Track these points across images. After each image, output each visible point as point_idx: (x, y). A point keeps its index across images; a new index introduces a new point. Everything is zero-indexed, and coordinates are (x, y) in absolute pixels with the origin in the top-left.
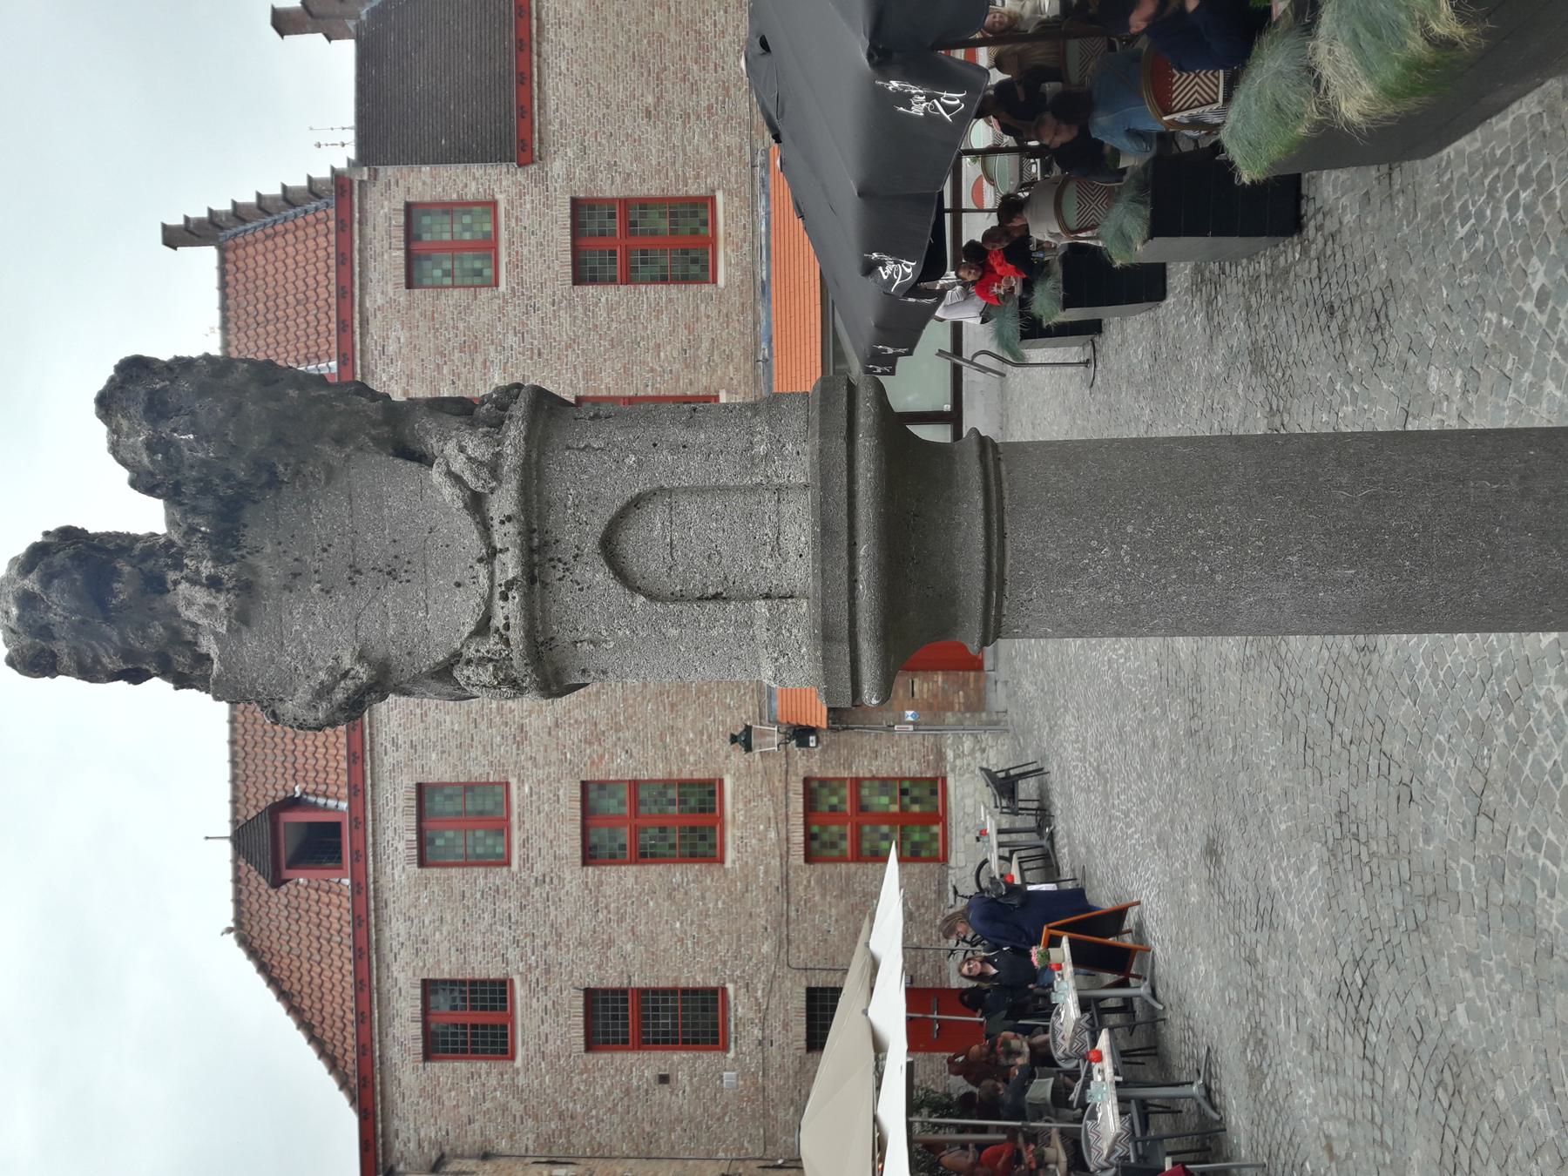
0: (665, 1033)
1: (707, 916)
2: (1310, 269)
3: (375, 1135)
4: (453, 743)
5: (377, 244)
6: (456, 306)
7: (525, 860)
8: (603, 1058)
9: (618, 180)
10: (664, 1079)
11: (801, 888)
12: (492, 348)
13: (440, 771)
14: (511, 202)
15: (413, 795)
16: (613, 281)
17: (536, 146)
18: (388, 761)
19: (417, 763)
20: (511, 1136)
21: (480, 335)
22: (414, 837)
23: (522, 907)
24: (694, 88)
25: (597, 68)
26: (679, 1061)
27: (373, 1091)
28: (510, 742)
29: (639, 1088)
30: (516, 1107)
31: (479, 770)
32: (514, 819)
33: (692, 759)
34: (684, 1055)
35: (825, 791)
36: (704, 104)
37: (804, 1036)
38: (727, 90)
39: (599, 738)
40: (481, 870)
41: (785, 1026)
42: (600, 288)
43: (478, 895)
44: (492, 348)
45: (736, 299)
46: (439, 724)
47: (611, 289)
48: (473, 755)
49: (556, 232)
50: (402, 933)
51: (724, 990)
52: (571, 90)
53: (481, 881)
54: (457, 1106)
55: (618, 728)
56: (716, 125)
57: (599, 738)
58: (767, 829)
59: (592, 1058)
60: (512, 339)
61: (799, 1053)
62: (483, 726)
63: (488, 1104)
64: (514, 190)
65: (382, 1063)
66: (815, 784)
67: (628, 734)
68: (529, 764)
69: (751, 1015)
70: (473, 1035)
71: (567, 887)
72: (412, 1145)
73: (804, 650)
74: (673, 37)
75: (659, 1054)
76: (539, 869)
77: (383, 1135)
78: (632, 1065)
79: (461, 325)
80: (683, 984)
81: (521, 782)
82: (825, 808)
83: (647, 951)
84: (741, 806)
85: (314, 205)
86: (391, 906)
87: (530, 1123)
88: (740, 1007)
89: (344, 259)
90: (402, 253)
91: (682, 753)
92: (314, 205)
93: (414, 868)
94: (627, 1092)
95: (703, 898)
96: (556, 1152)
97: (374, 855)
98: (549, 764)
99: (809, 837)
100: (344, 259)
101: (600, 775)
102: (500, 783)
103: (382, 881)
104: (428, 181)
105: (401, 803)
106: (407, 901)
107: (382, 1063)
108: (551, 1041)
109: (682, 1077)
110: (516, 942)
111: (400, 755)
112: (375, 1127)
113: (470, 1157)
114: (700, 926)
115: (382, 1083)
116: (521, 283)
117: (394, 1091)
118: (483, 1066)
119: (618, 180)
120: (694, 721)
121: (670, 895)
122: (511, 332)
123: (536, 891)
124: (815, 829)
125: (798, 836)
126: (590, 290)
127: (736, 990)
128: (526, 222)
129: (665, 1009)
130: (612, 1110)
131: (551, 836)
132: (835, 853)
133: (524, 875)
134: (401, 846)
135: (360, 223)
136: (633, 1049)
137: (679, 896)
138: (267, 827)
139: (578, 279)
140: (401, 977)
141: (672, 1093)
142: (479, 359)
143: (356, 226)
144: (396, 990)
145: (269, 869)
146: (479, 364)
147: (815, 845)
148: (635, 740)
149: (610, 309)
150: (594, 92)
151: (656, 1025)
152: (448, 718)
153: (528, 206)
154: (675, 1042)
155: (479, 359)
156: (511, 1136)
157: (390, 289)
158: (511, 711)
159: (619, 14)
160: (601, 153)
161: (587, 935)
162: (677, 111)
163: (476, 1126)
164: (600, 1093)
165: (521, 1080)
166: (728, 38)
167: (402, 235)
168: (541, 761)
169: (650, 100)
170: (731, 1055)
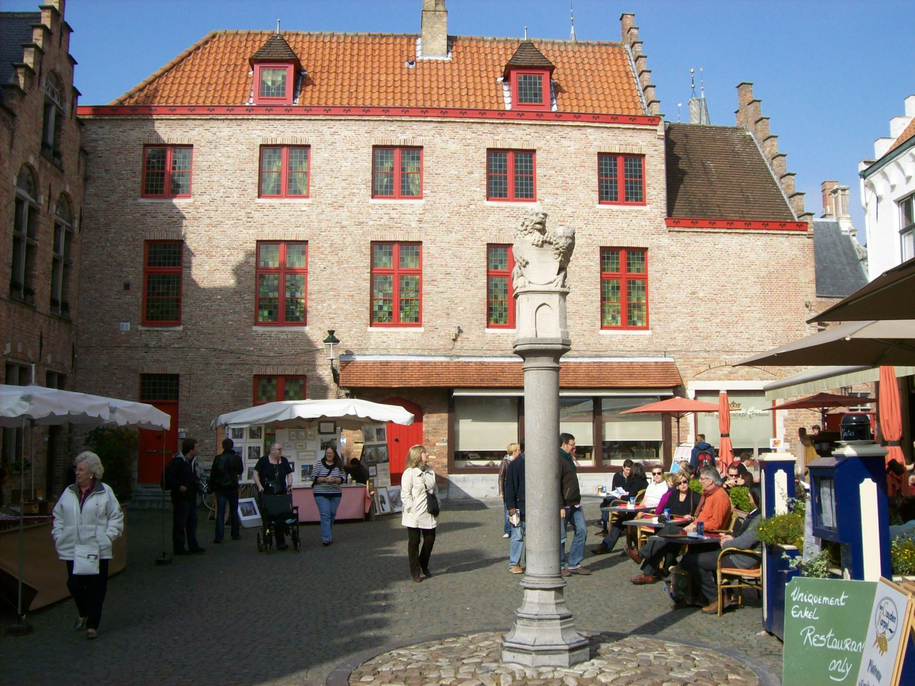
0: (154, 288)
1: (224, 315)
2: (198, 143)
3: (102, 115)
4: (334, 167)
5: (622, 137)
6: (588, 180)
7: (262, 207)
8: (141, 250)
9: (658, 275)
10: (127, 286)
11: (239, 372)
12: (565, 199)
13: (317, 158)
14: (645, 213)
15: (303, 143)
16: (602, 270)
17: (676, 229)
18: (325, 129)
19: (323, 146)
20: (96, 195)
21: (572, 192)
22: (278, 143)
23: (233, 204)
24: (707, 319)
25: (718, 265)
26: (136, 297)
27: (128, 115)
28: (334, 200)
29: (122, 272)
30: (114, 198)
31: (317, 181)
32: (287, 201)
33: (319, 307)
34: (141, 300)
35: (297, 388)
36: (699, 325)
37: (150, 372)
38: (706, 338)
39: (334, 252)
40: (257, 181)
41: (157, 361)
42: (599, 262)
43: (242, 179)
44: (565, 199)
45: (592, 341)
46: (345, 159)
47: (598, 268)
48: (326, 178)
49: (629, 238)
50: (222, 134)
51: (179, 324)
52: (706, 250)
53: (250, 181)
54: (116, 163)
55: (340, 263)
56: (687, 331)
57: (334, 252)
58: (275, 352)
59: (141, 243)
60: (569, 210)
61: (140, 369)
62: (344, 184)
63: (116, 181)
64: (652, 215)
65: (144, 120)
66: (301, 382)
67: (335, 269)
68: (319, 210)
69: (163, 340)
70: (158, 174)
71: (244, 231)
72: (94, 136)
73: (616, 649)
74: (734, 309)
75: (141, 285)
76: (256, 215)
77: (101, 120)
78: (136, 268)
79: (577, 182)
80: (184, 299)
81: (309, 205)
82: (287, 388)
83: (204, 278)
84: (290, 336)
85: (644, 101)
86: (239, 128)
87: (104, 206)
88: (169, 333)
89: (614, 118)
90: (617, 151)
91: (323, 301)
92: (644, 101)
93: (260, 142)
94: (120, 265)
95: (235, 313)
96: (86, 221)
97: (269, 119)
98: (320, 221)
99: (270, 378)
100: (614, 118)
101: (311, 252)
102: (308, 193)
103: (253, 123)
104: (657, 168)
105: (299, 136)
106: (241, 137)
107: (144, 120)
108: (152, 220)
109: (128, 298)
110: (213, 200)
111: (327, 136)
112: (106, 115)
113: (86, 171)
114: (218, 310)
115: (132, 120)
116: (601, 217)
117: (128, 125)
118: (139, 179)
119: (658, 275)
120: (342, 309)
121: (237, 292)
122: (574, 210)
123: (243, 213)
124: (274, 382)
125: (270, 371)
126: (598, 256)
127: (178, 331)
128: (634, 221)
129: (168, 288)
130: (109, 255)
131: (275, 222)
132: (260, 394)
133: (253, 206)
134: (273, 135)
135: (634, 129)
136: (145, 269)
137: (237, 298)
138: (287, 57)
139: (603, 249)
140: (195, 133)
141: (118, 292)
142: (559, 191)
143: (632, 126)
144: (187, 129)
145: (263, 56)
146: (555, 191)
147: (265, 382)
148: (332, 273)
149: (587, 267)
150: (705, 263)
151: (159, 283)
152: (349, 164)
153: (643, 223)
154: (149, 294)
155: (559, 191)
156: (96, 195)
157: (597, 143)
158: (352, 201)
159: (746, 278)
160: (672, 265)
161: (215, 242)
162: (695, 309)
163: (104, 174)
164: (120, 248)
165: (130, 201)
166: (734, 339)
167: (628, 152)
168: (321, 217)
169: (701, 295)
170: (140, 328)
